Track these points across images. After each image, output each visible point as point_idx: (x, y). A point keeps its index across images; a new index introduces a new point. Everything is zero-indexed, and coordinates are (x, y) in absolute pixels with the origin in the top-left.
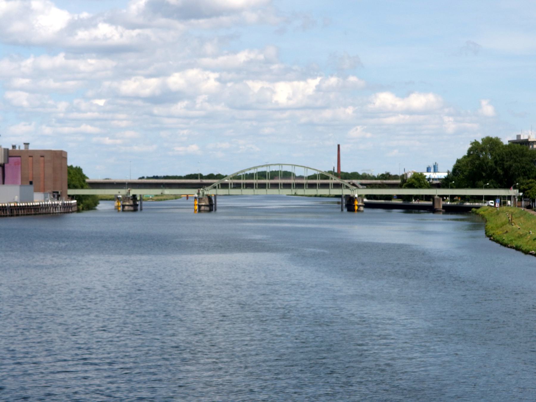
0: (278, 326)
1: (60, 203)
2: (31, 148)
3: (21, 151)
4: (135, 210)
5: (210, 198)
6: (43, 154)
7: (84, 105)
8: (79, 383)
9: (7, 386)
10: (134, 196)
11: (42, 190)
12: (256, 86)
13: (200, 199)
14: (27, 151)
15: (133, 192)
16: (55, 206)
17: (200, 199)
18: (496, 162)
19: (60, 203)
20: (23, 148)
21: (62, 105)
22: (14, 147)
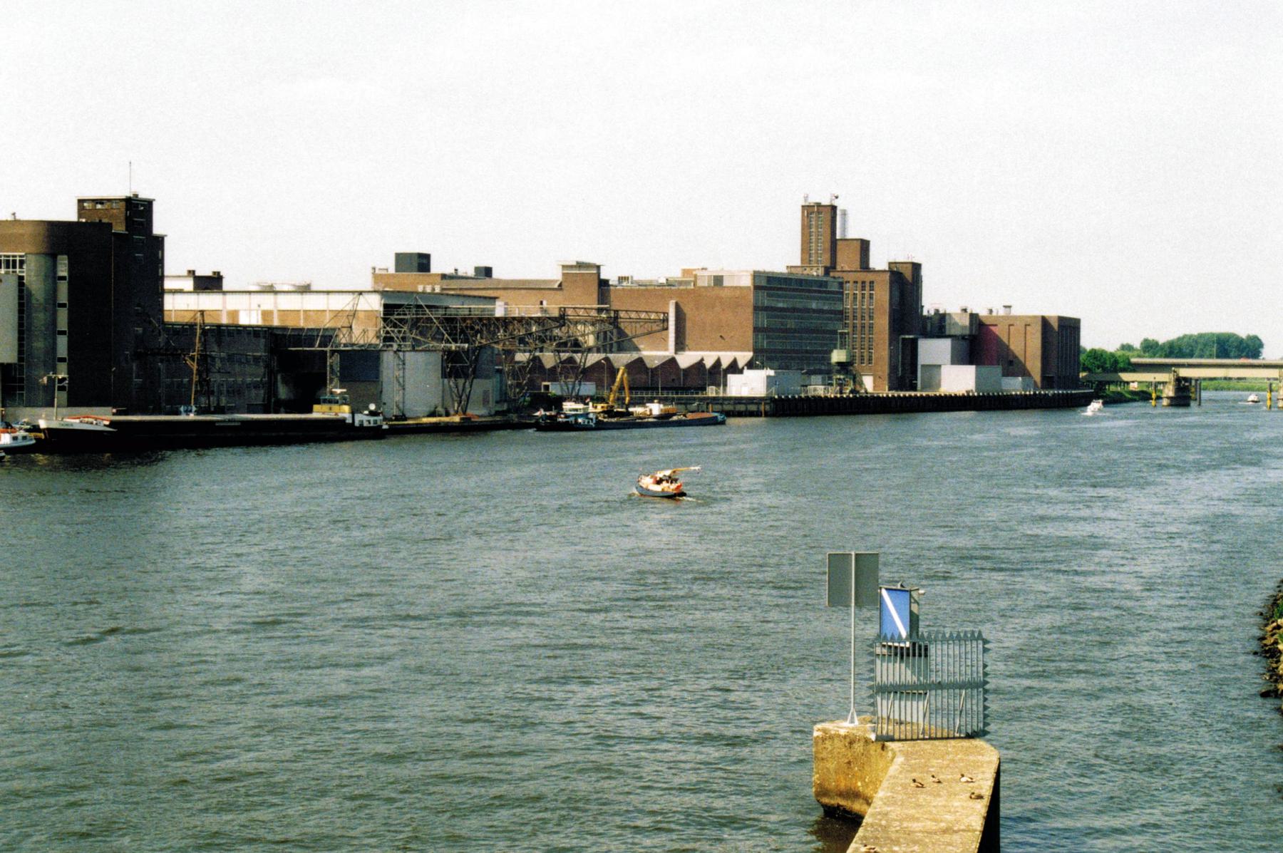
20: (1002, 312)
22: (991, 311)
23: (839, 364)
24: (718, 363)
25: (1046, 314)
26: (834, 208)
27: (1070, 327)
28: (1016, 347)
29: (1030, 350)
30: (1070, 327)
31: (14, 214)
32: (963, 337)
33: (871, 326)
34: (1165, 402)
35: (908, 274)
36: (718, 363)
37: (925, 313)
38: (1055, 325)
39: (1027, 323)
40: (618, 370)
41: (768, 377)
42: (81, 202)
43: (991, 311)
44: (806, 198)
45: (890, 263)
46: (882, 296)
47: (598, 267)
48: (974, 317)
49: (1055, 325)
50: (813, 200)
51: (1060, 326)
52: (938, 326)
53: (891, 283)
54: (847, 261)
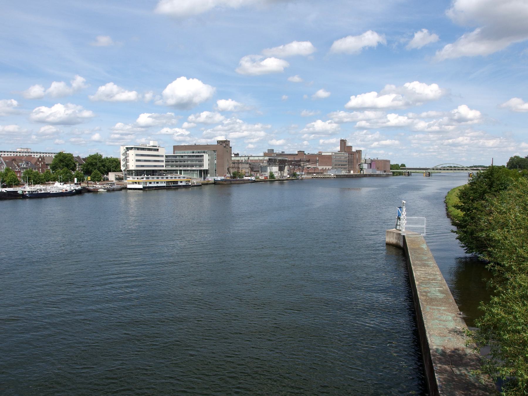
0: (58, 389)
1: (385, 174)
2: (378, 159)
3: (376, 160)
4: (409, 176)
5: (429, 172)
6: (381, 161)
7: (431, 147)
8: (235, 308)
9: (446, 219)
10: (408, 172)
11: (381, 170)
12: (482, 141)
13: (426, 173)
14: (377, 160)
15: (408, 171)
16: (384, 174)
17: (426, 173)
18: (516, 163)
19: (385, 174)
20: (376, 159)
21: (425, 148)
24: (326, 168)
27: (273, 150)
30: (273, 150)
36: (326, 168)
42: (229, 141)
47: (304, 151)
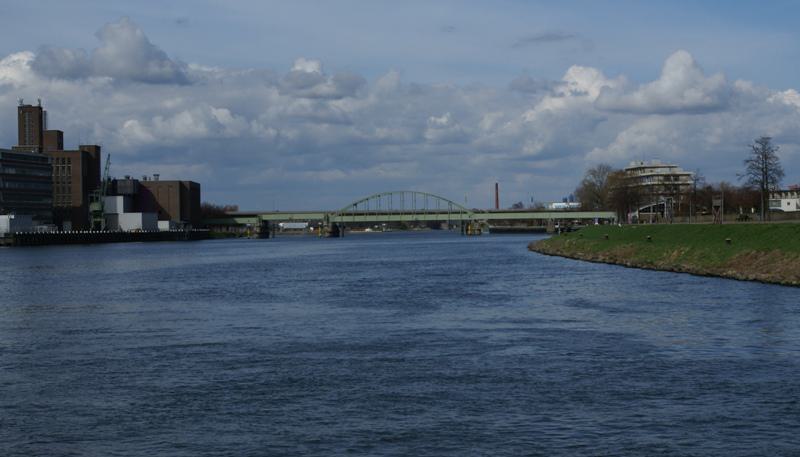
20: (153, 179)
23: (95, 211)
25: (183, 180)
26: (40, 108)
28: (162, 201)
29: (172, 203)
31: (698, 170)
32: (129, 195)
33: (70, 189)
34: (327, 235)
35: (93, 154)
37: (102, 180)
38: (188, 187)
39: (169, 184)
40: (125, 211)
41: (11, 219)
43: (145, 178)
44: (21, 101)
45: (80, 147)
46: (77, 168)
48: (136, 182)
49: (188, 187)
50: (25, 103)
51: (191, 188)
52: (113, 188)
53: (83, 158)
54: (50, 147)
